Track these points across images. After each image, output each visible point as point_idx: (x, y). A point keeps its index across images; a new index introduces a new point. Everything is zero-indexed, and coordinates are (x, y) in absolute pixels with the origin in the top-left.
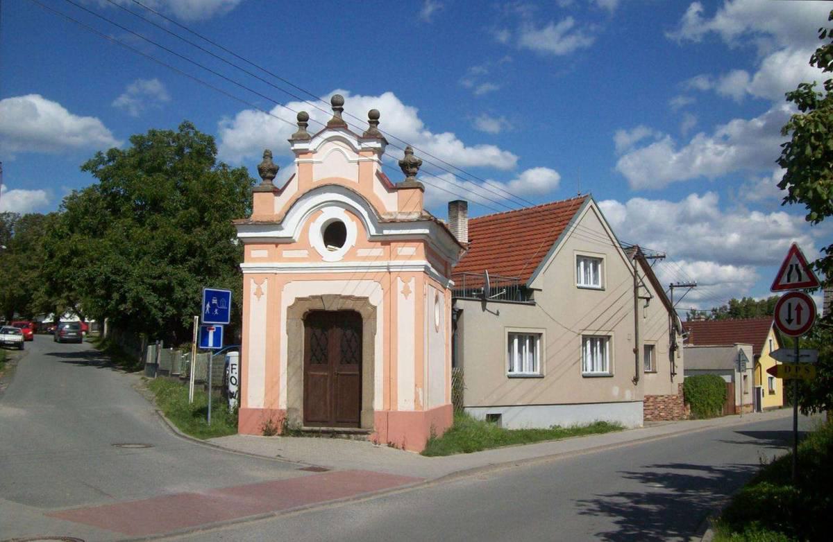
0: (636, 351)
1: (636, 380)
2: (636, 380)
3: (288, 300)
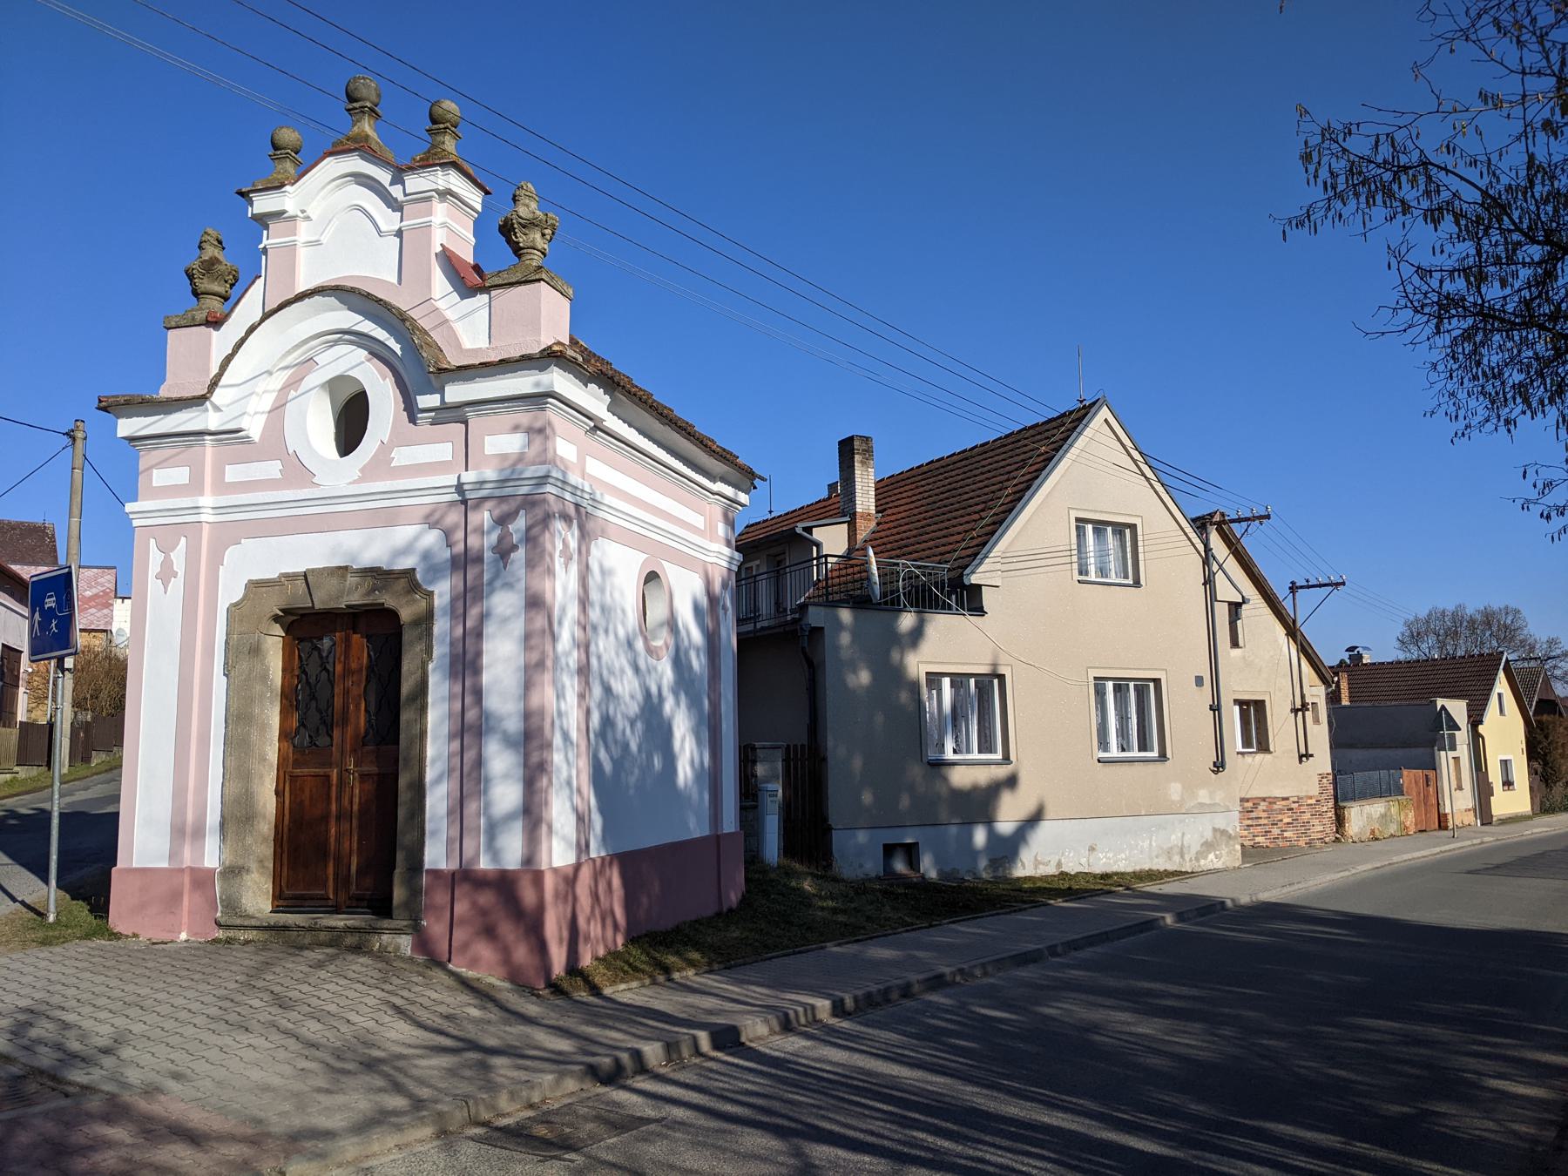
0: (1216, 708)
1: (1219, 766)
2: (1219, 766)
3: (231, 591)
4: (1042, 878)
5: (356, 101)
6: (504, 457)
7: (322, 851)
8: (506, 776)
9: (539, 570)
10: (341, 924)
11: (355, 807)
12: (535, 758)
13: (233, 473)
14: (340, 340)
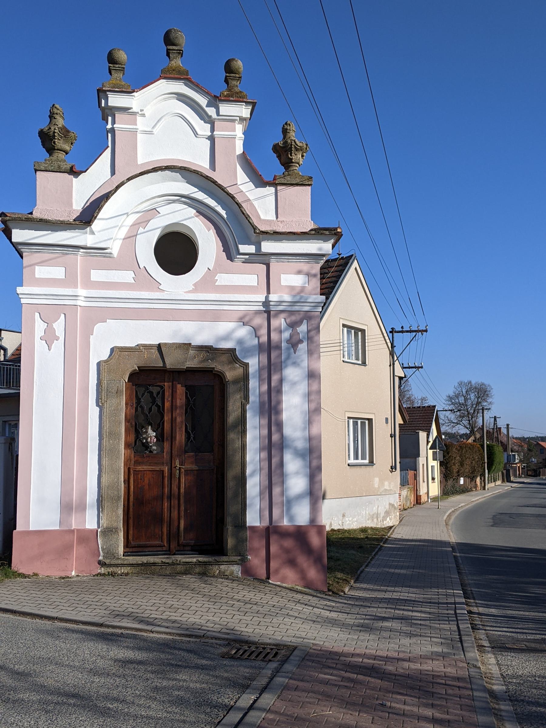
3: (100, 352)
4: (349, 531)
5: (174, 44)
6: (292, 288)
7: (158, 519)
8: (297, 473)
9: (315, 356)
10: (194, 560)
11: (182, 490)
12: (315, 463)
13: (96, 275)
14: (177, 200)
